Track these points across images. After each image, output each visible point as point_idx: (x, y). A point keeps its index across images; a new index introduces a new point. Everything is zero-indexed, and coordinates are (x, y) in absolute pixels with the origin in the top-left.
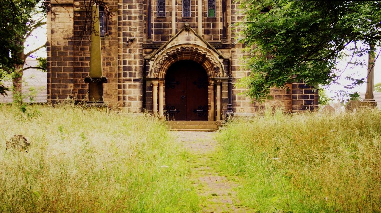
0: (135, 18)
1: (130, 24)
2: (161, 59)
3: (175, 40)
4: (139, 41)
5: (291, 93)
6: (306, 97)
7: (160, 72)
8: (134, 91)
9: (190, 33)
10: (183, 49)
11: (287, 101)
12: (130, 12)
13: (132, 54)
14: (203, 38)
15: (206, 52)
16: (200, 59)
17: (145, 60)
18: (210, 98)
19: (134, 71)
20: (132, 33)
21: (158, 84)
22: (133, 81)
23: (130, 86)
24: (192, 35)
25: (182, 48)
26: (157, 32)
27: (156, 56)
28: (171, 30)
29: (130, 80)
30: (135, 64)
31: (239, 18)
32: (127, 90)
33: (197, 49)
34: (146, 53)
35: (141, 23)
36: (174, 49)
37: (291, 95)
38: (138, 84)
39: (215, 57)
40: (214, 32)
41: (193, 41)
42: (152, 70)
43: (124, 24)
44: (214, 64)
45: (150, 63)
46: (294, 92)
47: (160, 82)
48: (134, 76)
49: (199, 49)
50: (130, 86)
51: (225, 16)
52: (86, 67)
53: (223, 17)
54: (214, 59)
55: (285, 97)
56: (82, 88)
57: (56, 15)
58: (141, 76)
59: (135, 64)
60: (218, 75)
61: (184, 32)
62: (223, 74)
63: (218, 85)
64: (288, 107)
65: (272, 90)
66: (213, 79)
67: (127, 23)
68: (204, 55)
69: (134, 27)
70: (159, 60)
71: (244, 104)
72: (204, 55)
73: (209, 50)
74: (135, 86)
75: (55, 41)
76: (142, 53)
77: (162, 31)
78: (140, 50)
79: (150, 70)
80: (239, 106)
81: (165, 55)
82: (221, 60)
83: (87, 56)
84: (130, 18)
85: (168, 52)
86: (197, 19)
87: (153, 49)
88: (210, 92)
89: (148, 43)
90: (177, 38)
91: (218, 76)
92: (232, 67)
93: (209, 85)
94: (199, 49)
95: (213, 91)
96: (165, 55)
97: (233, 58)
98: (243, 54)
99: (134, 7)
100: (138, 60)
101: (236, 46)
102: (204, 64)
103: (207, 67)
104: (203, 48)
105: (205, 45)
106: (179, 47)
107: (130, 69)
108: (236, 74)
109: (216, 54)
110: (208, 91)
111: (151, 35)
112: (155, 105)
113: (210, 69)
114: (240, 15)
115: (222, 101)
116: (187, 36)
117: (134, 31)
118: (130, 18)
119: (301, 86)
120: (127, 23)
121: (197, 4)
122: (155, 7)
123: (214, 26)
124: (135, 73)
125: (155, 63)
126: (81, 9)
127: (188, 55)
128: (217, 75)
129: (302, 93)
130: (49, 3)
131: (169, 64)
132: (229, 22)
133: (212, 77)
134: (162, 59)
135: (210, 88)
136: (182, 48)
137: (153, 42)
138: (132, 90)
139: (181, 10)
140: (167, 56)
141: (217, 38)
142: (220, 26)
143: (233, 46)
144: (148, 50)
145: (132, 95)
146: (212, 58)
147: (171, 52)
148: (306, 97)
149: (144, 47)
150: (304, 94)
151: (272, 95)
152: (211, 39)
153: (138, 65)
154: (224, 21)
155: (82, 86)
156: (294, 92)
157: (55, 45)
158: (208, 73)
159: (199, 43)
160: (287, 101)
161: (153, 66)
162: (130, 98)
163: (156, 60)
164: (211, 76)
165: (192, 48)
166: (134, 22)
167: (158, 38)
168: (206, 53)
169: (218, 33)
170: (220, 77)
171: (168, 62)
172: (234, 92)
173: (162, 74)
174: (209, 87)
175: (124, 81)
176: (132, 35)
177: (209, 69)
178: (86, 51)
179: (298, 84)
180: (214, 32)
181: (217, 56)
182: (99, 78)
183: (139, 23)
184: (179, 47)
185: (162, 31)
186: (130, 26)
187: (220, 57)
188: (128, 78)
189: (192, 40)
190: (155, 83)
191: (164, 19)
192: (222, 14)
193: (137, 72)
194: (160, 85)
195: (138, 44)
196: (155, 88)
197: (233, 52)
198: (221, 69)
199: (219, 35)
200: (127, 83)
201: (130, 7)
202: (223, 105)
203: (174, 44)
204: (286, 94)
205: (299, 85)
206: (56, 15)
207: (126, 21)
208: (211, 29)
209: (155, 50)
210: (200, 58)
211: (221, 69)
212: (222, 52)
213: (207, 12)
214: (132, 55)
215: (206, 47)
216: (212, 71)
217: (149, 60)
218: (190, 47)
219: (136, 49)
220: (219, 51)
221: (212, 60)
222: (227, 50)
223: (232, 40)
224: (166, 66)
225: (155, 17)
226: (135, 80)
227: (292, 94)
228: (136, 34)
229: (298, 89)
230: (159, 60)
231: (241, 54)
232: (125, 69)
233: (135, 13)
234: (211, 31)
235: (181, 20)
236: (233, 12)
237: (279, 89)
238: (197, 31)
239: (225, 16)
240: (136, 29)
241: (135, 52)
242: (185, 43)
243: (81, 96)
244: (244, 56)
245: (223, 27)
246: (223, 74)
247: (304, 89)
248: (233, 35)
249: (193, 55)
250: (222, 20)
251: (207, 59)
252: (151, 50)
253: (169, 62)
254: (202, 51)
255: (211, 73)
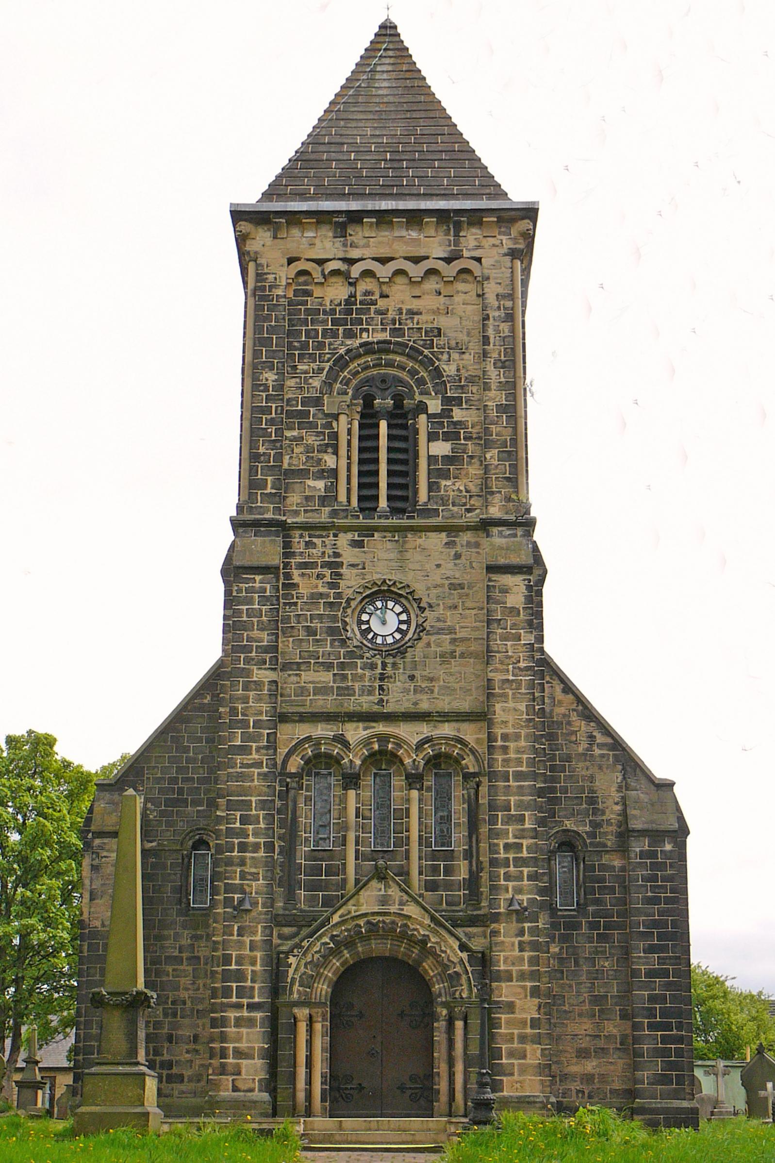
0: (256, 847)
1: (242, 863)
2: (316, 952)
3: (351, 902)
4: (264, 905)
5: (631, 1042)
6: (665, 1053)
7: (316, 985)
8: (248, 1033)
9: (390, 887)
10: (371, 927)
11: (621, 1062)
12: (244, 834)
13: (245, 938)
14: (420, 900)
15: (427, 933)
16: (413, 952)
17: (279, 953)
18: (442, 1052)
19: (249, 984)
20: (248, 885)
21: (311, 1016)
22: (245, 1007)
23: (237, 1019)
24: (394, 892)
25: (368, 922)
26: (312, 887)
27: (305, 944)
28: (344, 881)
29: (239, 1006)
30: (253, 963)
31: (507, 847)
32: (231, 1030)
33: (406, 925)
34: (280, 936)
35: (269, 859)
36: (350, 927)
37: (631, 1048)
38: (258, 1015)
39: (451, 947)
40: (448, 886)
41: (397, 907)
42: (293, 978)
43: (229, 862)
44: (448, 966)
45: (290, 961)
46: (636, 1040)
47: (314, 1011)
48: (248, 994)
49: (412, 927)
50: (239, 1022)
51: (474, 845)
52: (165, 979)
53: (471, 847)
54: (448, 951)
55: (617, 1052)
56: (154, 1029)
57: (102, 857)
58: (266, 995)
59: (253, 963)
60: (458, 993)
61: (374, 883)
62: (470, 990)
63: (457, 1019)
64: (626, 1076)
65: (586, 1035)
66: (445, 1005)
67: (236, 861)
68: (424, 941)
69: (253, 870)
70: (313, 956)
71: (523, 1070)
72: (424, 941)
73: (436, 930)
74: (251, 1023)
75: (97, 919)
76: (271, 935)
77: (323, 884)
78: (265, 927)
79: (289, 980)
80: (512, 1074)
81: (328, 940)
82: (464, 955)
83: (167, 954)
84: (243, 848)
85: (335, 933)
86: (408, 852)
87: (300, 927)
88: (440, 1037)
89: (287, 912)
90: (356, 897)
91: (457, 995)
92: (491, 971)
93: (438, 1020)
94: (412, 927)
95: (445, 1036)
96: (328, 940)
97: (494, 949)
98: (520, 938)
99: (252, 819)
100: (259, 954)
101: (503, 918)
102: (424, 964)
103: (432, 974)
104: (421, 924)
105: (426, 915)
106: (362, 922)
107: (239, 976)
108: (505, 992)
109: (453, 938)
110: (433, 1037)
111: (295, 894)
112: (302, 1071)
113: (439, 977)
114: (510, 730)
115: (468, 1062)
116: (382, 893)
117: (250, 880)
118: (243, 848)
119: (651, 1026)
120: (236, 861)
121: (408, 817)
122: (308, 825)
123: (448, 871)
124: (253, 988)
125: (303, 962)
126: (159, 844)
127: (385, 941)
128: (454, 994)
129: (655, 1042)
130: (89, 831)
131: (338, 964)
132: (485, 859)
133: (444, 999)
134: (319, 951)
135: (438, 1028)
136: (368, 922)
137: (302, 911)
138: (244, 1030)
139: (368, 831)
140: (332, 945)
141: (456, 899)
142: (462, 872)
143: (496, 918)
144: (287, 930)
145: (243, 1045)
146: (444, 948)
147: (341, 932)
148: (665, 1053)
149: (276, 920)
150: (660, 1045)
151: (586, 1048)
152: (441, 904)
153: (258, 968)
154: (471, 856)
155: (154, 1025)
156: (636, 1040)
157: (96, 927)
158: (433, 989)
159: (411, 910)
160: (621, 1062)
161: (296, 970)
162: (239, 1054)
163: (304, 954)
164: (440, 995)
165: (393, 922)
166: (253, 858)
167: (312, 900)
168: (428, 936)
169: (457, 887)
170: (462, 998)
171: (334, 961)
172: (499, 1039)
173: (319, 990)
174: (435, 1024)
175: (224, 1007)
176: (248, 889)
177: (434, 979)
178: (167, 943)
179: (646, 1021)
180: (448, 886)
181: (456, 945)
182: (127, 993)
183: (264, 860)
184: (362, 922)
185: (323, 884)
186: (243, 868)
187: (463, 947)
188: (234, 1000)
189: (394, 903)
190: (302, 1013)
191: (328, 853)
192: (468, 840)
193: (257, 986)
194: (314, 1019)
195: (260, 913)
196: (302, 1027)
197: (494, 933)
198: (464, 977)
199: (503, 1031)
200: (232, 1015)
201: (244, 820)
202: (470, 1072)
203: (349, 912)
204: (618, 1046)
205: (648, 1022)
206: (102, 857)
207: (233, 854)
208: (442, 877)
209: (304, 929)
210: (414, 950)
211: (464, 977)
212: (466, 934)
213: (431, 837)
214: (247, 940)
215: (427, 921)
216: (443, 983)
217: (287, 954)
218: (388, 921)
219: (257, 927)
220: (460, 932)
221: (443, 955)
222: (480, 929)
223: (493, 903)
224: (329, 972)
225: (306, 849)
226: (252, 1007)
227: (633, 1044)
228: (257, 886)
229: (647, 1033)
230: (313, 956)
231: (513, 939)
232: (227, 976)
233: (256, 834)
234: (442, 882)
235: (370, 857)
236: (494, 834)
237: (602, 1034)
238: (407, 882)
239: (474, 845)
240: (259, 874)
241: (255, 933)
242: (376, 909)
243: (151, 1048)
244: (521, 943)
245: (470, 871)
246: (470, 990)
247: (659, 1033)
248: (494, 889)
249: (395, 943)
250: (468, 855)
251: (432, 953)
252: (294, 929)
253: (337, 961)
254: (419, 932)
255: (440, 988)
